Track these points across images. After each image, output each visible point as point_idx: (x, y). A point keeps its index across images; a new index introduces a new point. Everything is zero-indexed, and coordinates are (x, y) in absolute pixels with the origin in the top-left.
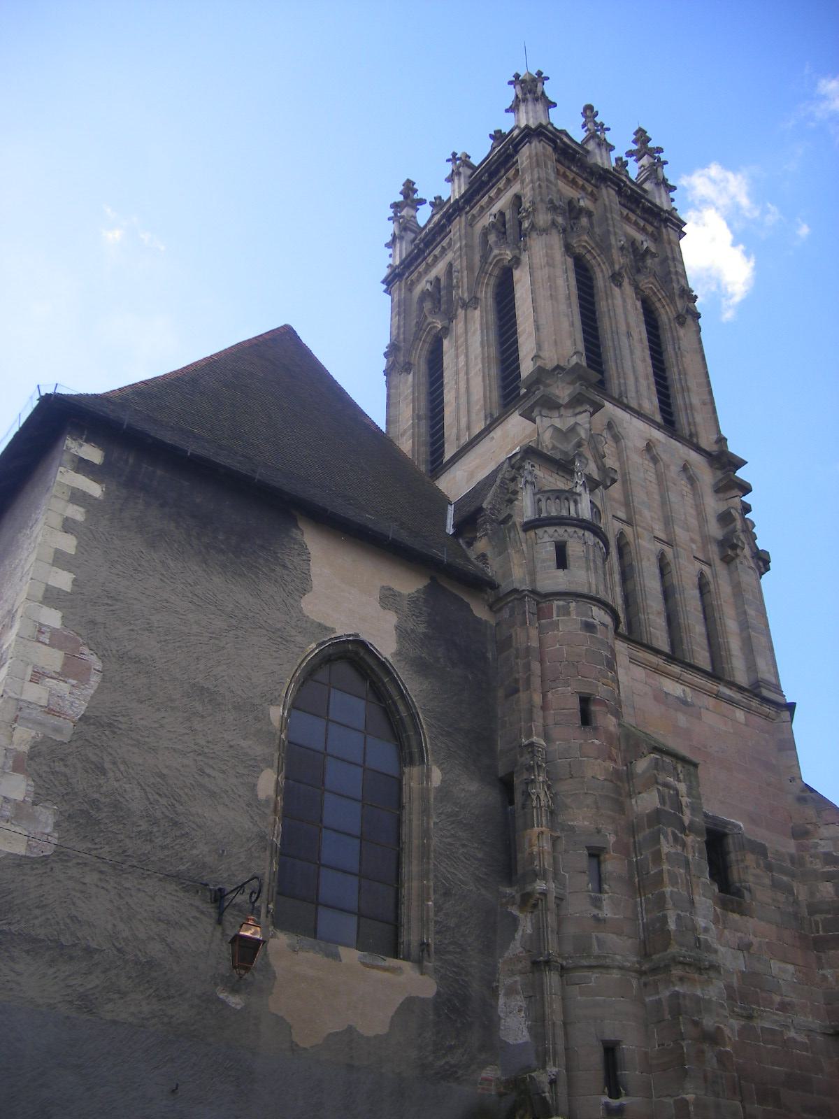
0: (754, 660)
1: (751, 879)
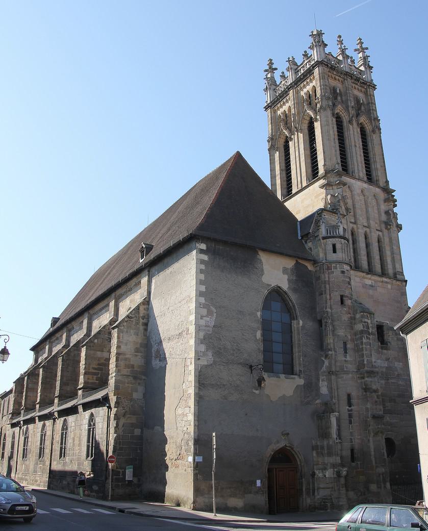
0: (395, 265)
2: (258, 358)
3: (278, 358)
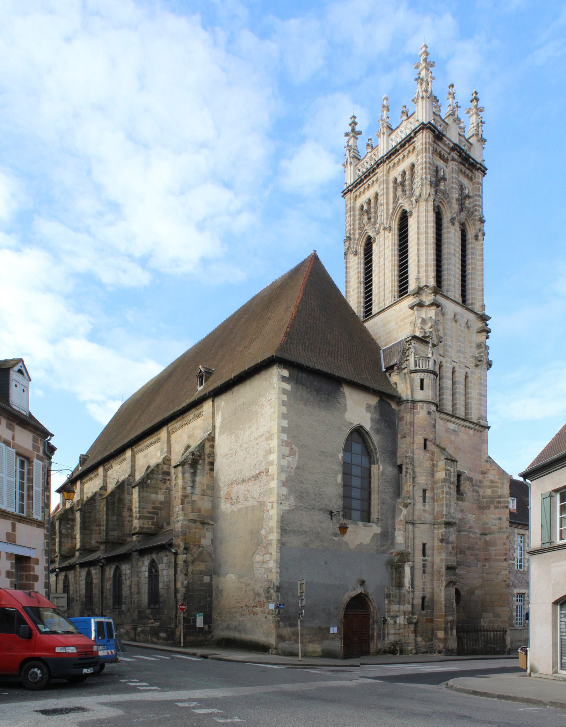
1: (466, 489)
2: (337, 504)
3: (356, 504)
